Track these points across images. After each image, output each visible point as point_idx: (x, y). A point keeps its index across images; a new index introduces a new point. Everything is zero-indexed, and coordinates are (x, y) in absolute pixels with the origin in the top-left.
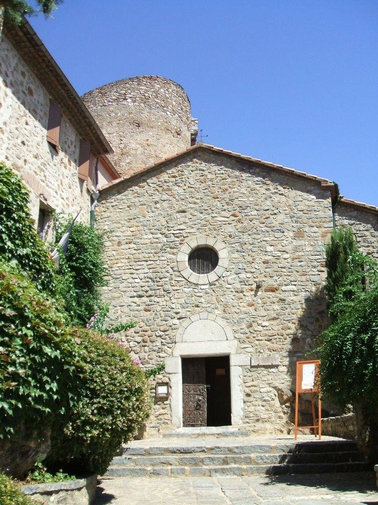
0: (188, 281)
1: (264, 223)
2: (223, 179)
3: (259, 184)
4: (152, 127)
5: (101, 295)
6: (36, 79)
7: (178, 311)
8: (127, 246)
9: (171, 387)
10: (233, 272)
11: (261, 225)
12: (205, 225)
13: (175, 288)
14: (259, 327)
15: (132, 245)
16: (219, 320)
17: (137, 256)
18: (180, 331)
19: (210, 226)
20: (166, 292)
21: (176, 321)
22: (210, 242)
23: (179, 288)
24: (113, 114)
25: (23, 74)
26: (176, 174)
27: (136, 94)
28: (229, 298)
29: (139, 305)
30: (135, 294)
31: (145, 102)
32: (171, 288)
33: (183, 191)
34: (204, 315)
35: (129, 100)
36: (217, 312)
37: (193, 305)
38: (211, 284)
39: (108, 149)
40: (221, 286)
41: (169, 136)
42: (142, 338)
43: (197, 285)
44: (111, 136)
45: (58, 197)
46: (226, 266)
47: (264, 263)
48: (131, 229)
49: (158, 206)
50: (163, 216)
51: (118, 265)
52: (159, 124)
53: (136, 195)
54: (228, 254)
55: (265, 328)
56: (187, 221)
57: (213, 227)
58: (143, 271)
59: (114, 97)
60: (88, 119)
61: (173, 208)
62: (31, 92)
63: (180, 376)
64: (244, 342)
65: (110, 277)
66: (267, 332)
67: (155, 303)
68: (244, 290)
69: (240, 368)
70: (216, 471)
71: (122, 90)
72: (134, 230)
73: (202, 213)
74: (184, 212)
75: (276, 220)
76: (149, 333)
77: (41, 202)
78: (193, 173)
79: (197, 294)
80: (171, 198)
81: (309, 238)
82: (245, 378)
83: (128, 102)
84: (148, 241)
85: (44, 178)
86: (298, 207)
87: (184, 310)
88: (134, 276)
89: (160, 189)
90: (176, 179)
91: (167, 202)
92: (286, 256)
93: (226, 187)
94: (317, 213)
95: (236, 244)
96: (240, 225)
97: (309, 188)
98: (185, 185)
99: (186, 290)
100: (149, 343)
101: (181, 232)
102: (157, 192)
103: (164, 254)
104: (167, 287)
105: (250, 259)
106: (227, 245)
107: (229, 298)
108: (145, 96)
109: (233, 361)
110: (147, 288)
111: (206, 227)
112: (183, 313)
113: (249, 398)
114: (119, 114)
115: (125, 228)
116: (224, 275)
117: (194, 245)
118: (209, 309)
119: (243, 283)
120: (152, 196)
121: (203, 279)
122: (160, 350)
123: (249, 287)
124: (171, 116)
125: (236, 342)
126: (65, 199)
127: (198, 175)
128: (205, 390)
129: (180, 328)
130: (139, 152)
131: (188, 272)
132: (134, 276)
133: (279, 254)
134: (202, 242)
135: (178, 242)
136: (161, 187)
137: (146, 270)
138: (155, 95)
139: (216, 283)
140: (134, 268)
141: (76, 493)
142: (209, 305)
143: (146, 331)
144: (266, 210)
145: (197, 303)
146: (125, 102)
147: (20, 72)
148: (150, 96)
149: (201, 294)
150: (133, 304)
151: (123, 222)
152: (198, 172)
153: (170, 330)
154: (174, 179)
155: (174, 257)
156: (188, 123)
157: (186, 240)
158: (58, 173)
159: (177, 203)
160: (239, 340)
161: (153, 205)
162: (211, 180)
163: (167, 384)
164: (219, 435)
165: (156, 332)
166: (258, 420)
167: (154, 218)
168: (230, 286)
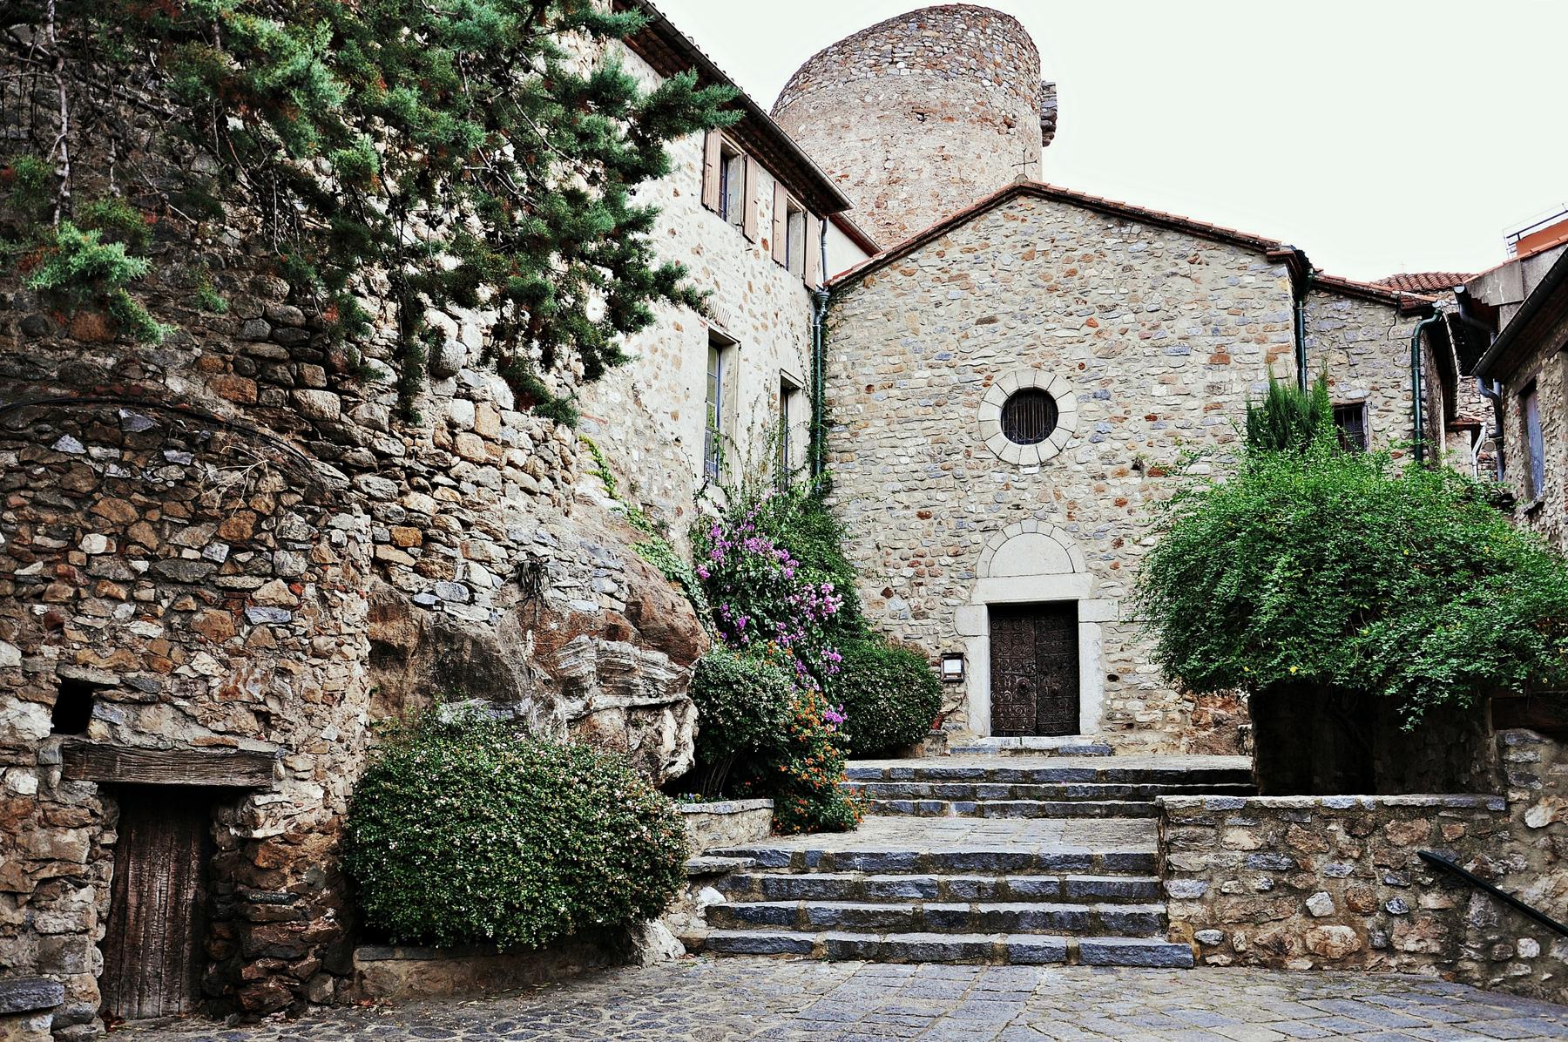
4: (951, 119)
7: (980, 517)
8: (883, 393)
10: (1086, 440)
11: (1143, 343)
12: (1032, 346)
13: (975, 473)
14: (1137, 547)
15: (893, 392)
16: (1058, 533)
17: (904, 413)
19: (1041, 348)
22: (1042, 383)
24: (869, 99)
26: (975, 245)
27: (915, 49)
28: (1080, 491)
29: (907, 507)
30: (899, 486)
33: (989, 279)
35: (901, 65)
38: (1043, 464)
40: (1063, 468)
41: (988, 132)
42: (913, 570)
43: (1016, 466)
44: (867, 144)
45: (746, 315)
47: (1148, 418)
48: (891, 360)
49: (941, 311)
51: (868, 431)
52: (967, 109)
53: (899, 291)
56: (999, 339)
58: (914, 441)
64: (1106, 576)
68: (1108, 474)
69: (1097, 626)
70: (993, 808)
71: (886, 43)
73: (1025, 322)
74: (991, 320)
77: (711, 331)
78: (1009, 241)
81: (1239, 366)
86: (1219, 302)
87: (992, 516)
88: (898, 451)
89: (945, 277)
92: (1192, 403)
93: (1074, 265)
94: (1258, 313)
95: (1093, 383)
96: (1101, 344)
97: (1242, 261)
99: (998, 477)
100: (927, 579)
101: (984, 361)
102: (939, 284)
103: (953, 408)
104: (959, 471)
105: (1120, 412)
106: (1076, 385)
107: (1080, 491)
109: (1083, 615)
110: (922, 475)
112: (990, 519)
115: (879, 360)
117: (1011, 388)
118: (1040, 514)
119: (1105, 461)
121: (1028, 453)
122: (948, 592)
123: (1117, 468)
124: (992, 89)
125: (1090, 576)
126: (759, 316)
130: (924, 175)
131: (999, 441)
132: (898, 451)
133: (1178, 400)
137: (921, 440)
138: (954, 46)
139: (1054, 461)
141: (727, 819)
142: (1039, 505)
146: (892, 70)
148: (946, 50)
150: (897, 505)
151: (875, 348)
153: (967, 555)
154: (970, 256)
155: (973, 411)
156: (1033, 96)
158: (742, 271)
159: (977, 303)
162: (1045, 253)
163: (960, 656)
164: (1054, 752)
166: (1130, 726)
167: (935, 336)
168: (1080, 468)
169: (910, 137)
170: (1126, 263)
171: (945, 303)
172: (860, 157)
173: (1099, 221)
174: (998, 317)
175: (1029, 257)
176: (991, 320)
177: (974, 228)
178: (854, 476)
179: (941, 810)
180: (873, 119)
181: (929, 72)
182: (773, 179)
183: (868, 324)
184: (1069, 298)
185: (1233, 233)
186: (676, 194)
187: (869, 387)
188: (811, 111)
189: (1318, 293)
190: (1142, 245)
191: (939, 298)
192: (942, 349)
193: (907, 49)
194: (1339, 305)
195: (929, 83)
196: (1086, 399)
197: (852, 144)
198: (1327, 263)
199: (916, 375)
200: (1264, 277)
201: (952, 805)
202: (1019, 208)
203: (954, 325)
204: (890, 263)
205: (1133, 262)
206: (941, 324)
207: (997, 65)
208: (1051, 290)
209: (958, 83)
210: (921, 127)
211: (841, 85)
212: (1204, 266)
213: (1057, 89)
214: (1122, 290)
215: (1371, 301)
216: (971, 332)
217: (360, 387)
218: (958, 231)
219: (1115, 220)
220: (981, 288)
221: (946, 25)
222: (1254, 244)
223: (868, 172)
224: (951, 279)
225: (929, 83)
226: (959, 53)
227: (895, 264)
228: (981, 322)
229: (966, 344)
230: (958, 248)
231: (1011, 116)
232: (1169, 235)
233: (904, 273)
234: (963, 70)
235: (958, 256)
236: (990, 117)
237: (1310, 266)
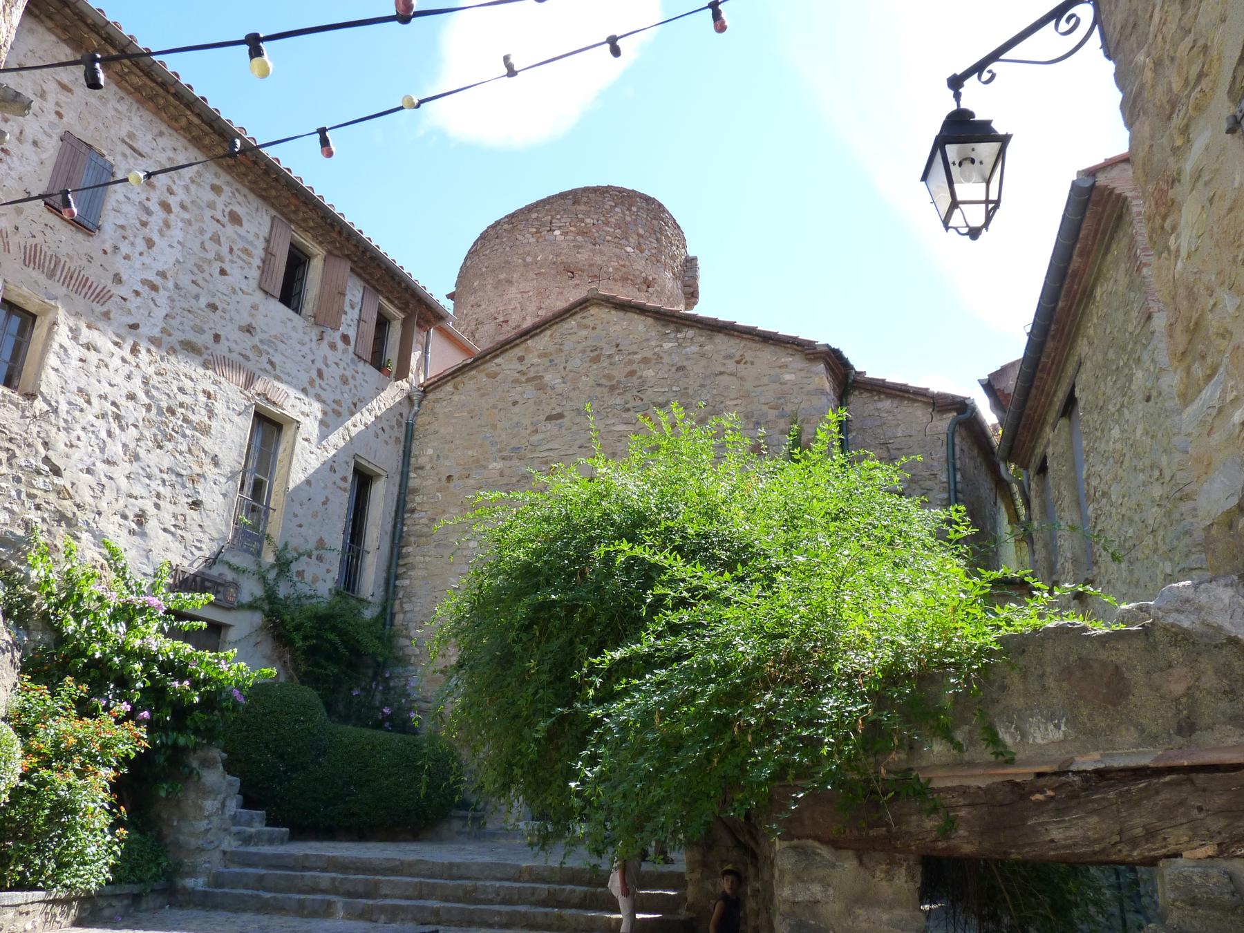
5: (413, 568)
6: (251, 197)
25: (216, 189)
35: (557, 232)
39: (444, 316)
44: (525, 296)
52: (611, 270)
62: (235, 219)
85: (269, 367)
93: (635, 367)
97: (783, 360)
147: (208, 188)
162: (609, 356)
167: (510, 431)
169: (561, 290)
170: (680, 364)
171: (521, 402)
172: (518, 306)
173: (659, 328)
174: (565, 414)
175: (596, 360)
176: (560, 416)
177: (551, 336)
178: (427, 559)
179: (326, 911)
180: (531, 275)
181: (580, 238)
182: (362, 283)
183: (453, 421)
184: (628, 396)
185: (776, 334)
186: (223, 272)
187: (449, 477)
188: (484, 269)
189: (861, 394)
190: (695, 348)
191: (517, 397)
192: (514, 444)
193: (563, 220)
194: (880, 405)
195: (579, 247)
197: (514, 296)
198: (866, 363)
199: (490, 467)
200: (803, 374)
201: (339, 902)
202: (591, 318)
203: (527, 422)
204: (477, 366)
205: (686, 363)
206: (515, 420)
207: (639, 236)
208: (612, 389)
209: (605, 249)
210: (570, 282)
211: (508, 249)
212: (749, 365)
213: (700, 263)
214: (675, 389)
215: (909, 399)
216: (541, 427)
217: (639, 641)
218: (537, 338)
219: (672, 327)
220: (553, 388)
221: (596, 202)
222: (793, 343)
223: (524, 318)
224: (528, 381)
225: (579, 247)
226: (607, 224)
227: (482, 368)
228: (549, 418)
229: (535, 438)
230: (536, 353)
231: (651, 278)
232: (720, 339)
233: (488, 376)
234: (608, 238)
235: (536, 361)
236: (631, 277)
237: (851, 367)
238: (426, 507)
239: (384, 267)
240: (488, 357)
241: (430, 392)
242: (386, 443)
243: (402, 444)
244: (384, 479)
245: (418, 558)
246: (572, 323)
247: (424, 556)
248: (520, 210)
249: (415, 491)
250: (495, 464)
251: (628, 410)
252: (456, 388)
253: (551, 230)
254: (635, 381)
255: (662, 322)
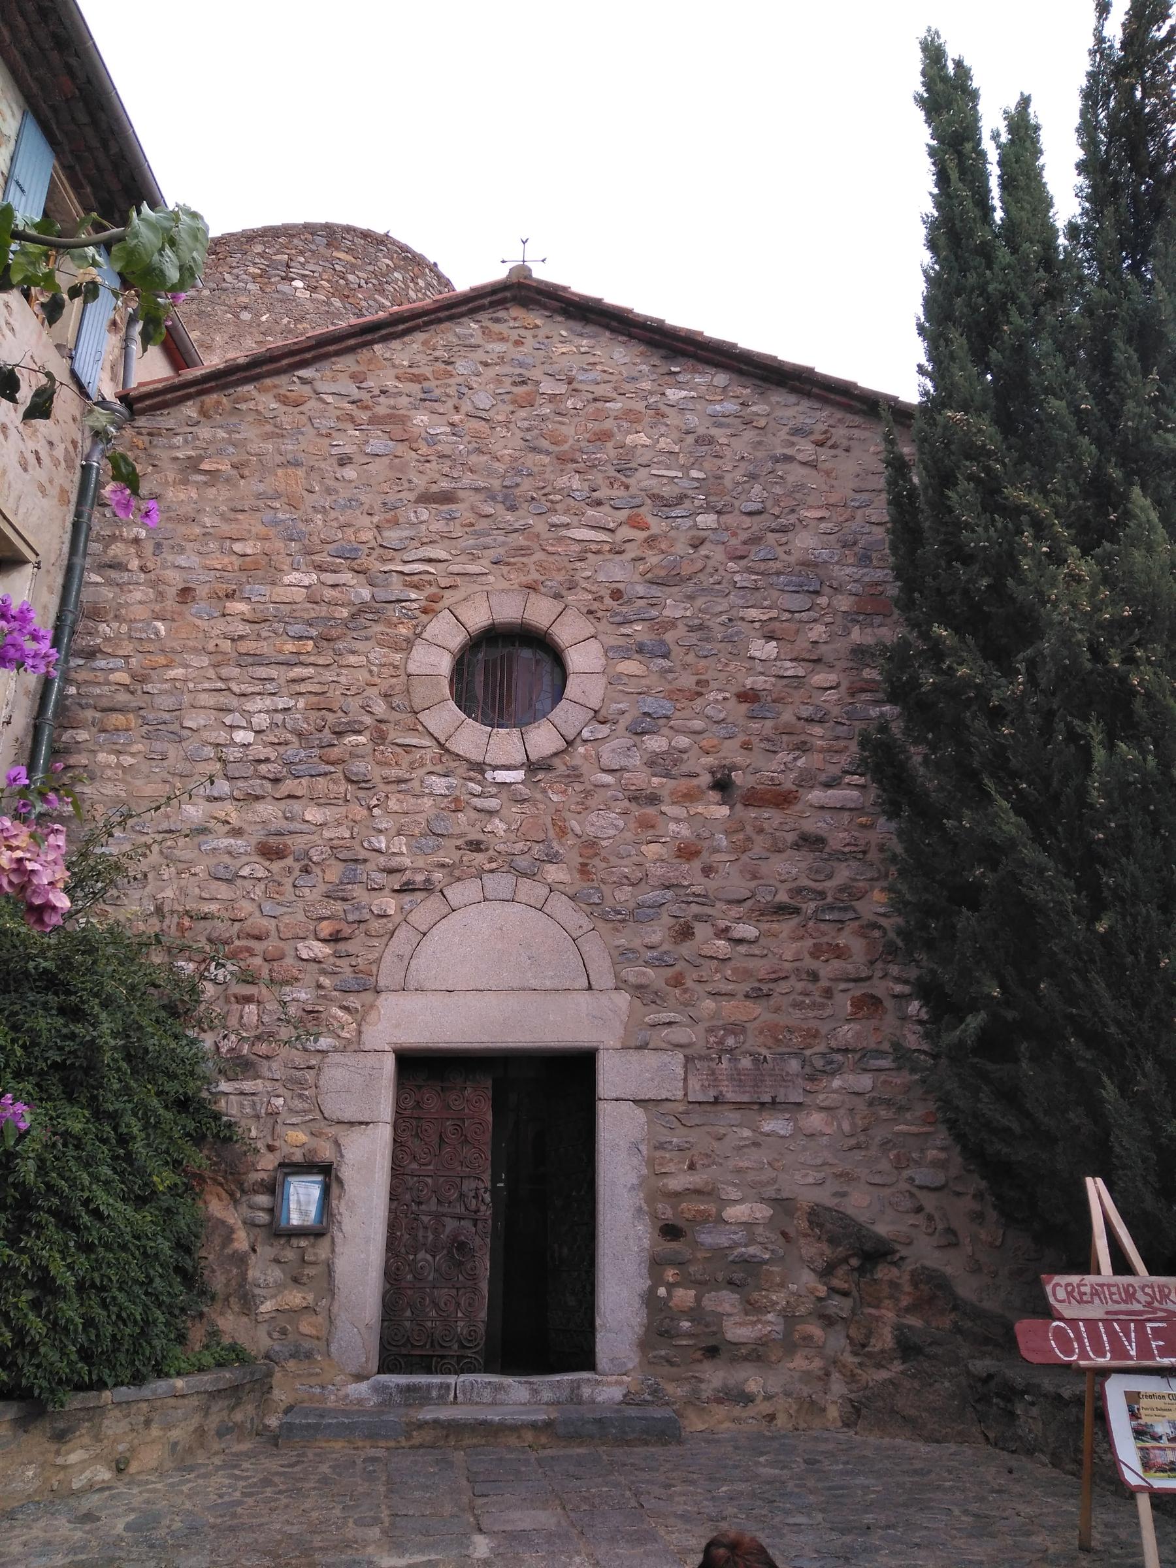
0: (447, 751)
1: (742, 557)
2: (595, 400)
3: (728, 426)
9: (340, 1182)
13: (393, 773)
16: (560, 905)
18: (403, 938)
19: (539, 556)
20: (355, 786)
21: (389, 904)
23: (407, 776)
24: (246, 316)
26: (427, 371)
31: (347, 297)
32: (376, 773)
33: (448, 429)
34: (501, 883)
36: (553, 873)
37: (459, 842)
40: (574, 775)
43: (480, 767)
46: (595, 703)
50: (366, 507)
51: (172, 674)
54: (603, 661)
55: (742, 949)
57: (551, 558)
59: (251, 270)
60: (77, 55)
61: (406, 485)
63: (384, 1134)
65: (131, 716)
66: (751, 964)
67: (304, 827)
72: (249, 551)
74: (447, 498)
75: (786, 548)
76: (270, 945)
78: (491, 372)
79: (476, 802)
80: (401, 449)
82: (658, 1154)
83: (296, 289)
84: (300, 595)
89: (364, 416)
90: (426, 384)
91: (386, 460)
93: (609, 424)
98: (456, 408)
103: (358, 645)
108: (346, 280)
111: (524, 560)
113: (674, 1245)
114: (264, 318)
116: (586, 734)
117: (478, 618)
120: (329, 435)
125: (623, 999)
127: (508, 380)
128: (487, 1197)
129: (403, 933)
134: (508, 611)
135: (415, 605)
136: (367, 408)
140: (236, 689)
143: (258, 938)
144: (750, 514)
145: (475, 835)
146: (283, 287)
148: (363, 283)
149: (493, 803)
152: (507, 369)
157: (449, 598)
160: (639, 990)
161: (329, 466)
165: (300, 945)
166: (712, 1352)
170: (701, 431)
174: (461, 494)
176: (447, 498)
177: (425, 343)
178: (127, 760)
181: (336, 302)
184: (597, 477)
196: (624, 652)
205: (714, 431)
214: (694, 473)
218: (396, 344)
224: (374, 420)
226: (382, 292)
227: (268, 382)
228: (425, 499)
229: (392, 536)
238: (127, 648)
239: (114, 150)
240: (285, 362)
241: (143, 412)
242: (42, 489)
243: (72, 508)
244: (29, 569)
245: (102, 757)
246: (471, 328)
247: (119, 753)
248: (231, 235)
249: (96, 614)
250: (297, 575)
251: (599, 503)
252: (204, 413)
253: (288, 279)
254: (608, 452)
255: (663, 352)
